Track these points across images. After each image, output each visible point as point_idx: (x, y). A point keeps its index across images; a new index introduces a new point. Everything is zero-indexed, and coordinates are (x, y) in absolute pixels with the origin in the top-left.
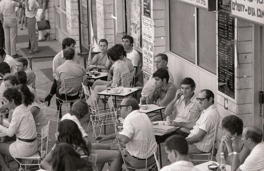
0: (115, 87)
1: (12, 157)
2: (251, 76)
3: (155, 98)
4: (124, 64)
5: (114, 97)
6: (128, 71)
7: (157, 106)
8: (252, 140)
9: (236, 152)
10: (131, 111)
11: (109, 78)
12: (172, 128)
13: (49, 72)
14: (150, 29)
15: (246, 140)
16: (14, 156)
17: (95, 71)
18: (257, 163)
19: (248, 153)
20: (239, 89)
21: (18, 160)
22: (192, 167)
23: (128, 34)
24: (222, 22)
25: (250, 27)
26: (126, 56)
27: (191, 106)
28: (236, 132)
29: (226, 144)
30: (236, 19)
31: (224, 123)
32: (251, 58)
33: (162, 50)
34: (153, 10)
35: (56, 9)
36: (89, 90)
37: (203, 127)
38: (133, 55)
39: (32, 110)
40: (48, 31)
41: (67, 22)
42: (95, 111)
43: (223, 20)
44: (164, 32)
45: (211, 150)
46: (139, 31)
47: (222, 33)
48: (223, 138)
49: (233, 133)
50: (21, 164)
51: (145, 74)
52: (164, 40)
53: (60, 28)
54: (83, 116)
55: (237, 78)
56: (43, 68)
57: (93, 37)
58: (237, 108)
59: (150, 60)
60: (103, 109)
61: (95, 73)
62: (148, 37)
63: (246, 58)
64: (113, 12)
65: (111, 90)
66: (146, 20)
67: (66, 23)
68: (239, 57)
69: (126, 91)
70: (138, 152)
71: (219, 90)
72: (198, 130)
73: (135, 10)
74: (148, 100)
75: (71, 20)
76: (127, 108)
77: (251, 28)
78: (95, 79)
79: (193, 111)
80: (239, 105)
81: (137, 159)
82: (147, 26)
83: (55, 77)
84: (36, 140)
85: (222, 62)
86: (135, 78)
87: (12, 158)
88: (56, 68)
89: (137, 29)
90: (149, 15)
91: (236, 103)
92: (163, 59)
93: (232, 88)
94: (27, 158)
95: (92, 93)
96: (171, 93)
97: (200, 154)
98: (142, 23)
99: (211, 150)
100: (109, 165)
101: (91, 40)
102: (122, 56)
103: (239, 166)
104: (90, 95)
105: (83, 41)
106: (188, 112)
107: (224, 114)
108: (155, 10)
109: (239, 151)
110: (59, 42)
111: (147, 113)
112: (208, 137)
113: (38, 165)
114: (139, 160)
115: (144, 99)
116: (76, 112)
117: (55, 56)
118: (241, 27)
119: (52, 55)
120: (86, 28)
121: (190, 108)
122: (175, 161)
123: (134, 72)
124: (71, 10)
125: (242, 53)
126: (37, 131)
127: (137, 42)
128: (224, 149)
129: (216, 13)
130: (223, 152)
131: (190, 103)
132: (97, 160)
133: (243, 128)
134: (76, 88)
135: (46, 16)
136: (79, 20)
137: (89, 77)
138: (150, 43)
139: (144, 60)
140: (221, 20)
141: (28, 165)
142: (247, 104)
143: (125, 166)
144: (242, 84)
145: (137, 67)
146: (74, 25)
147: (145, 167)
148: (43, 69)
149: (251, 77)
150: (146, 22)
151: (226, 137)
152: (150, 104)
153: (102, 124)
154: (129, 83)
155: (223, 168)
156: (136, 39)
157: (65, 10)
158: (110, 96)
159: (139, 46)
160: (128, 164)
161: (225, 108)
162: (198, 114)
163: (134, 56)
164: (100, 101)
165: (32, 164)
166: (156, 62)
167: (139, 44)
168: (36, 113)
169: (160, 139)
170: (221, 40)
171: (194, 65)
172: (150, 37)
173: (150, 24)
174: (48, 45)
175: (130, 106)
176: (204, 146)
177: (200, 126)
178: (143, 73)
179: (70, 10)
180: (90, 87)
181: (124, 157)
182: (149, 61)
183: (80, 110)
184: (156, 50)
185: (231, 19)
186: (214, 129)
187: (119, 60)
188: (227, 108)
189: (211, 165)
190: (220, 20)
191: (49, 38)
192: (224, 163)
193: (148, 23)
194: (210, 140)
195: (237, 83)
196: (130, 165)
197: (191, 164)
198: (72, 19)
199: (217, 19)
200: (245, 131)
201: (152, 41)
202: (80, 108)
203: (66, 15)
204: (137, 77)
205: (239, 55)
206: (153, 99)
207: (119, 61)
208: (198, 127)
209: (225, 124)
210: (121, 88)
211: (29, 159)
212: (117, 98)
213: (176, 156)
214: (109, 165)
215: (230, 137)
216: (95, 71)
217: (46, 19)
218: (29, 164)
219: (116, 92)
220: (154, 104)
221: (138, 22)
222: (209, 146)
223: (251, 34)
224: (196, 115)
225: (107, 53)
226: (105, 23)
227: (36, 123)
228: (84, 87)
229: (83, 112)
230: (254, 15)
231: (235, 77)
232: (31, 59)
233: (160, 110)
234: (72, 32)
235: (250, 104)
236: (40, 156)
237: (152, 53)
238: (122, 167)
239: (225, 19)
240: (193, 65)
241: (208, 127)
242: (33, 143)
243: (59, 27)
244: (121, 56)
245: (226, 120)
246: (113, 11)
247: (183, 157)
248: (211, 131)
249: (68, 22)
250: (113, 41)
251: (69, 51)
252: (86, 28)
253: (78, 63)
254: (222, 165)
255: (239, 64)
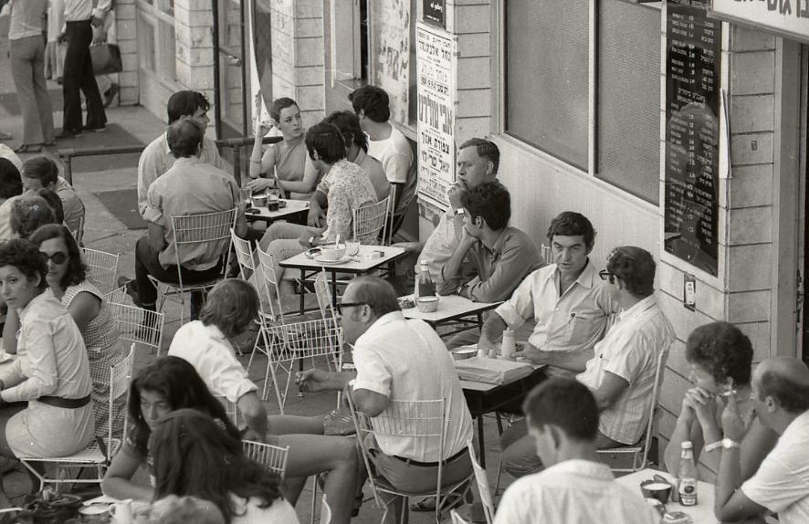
0: (335, 244)
1: (14, 458)
2: (768, 203)
3: (465, 272)
4: (360, 171)
5: (330, 273)
6: (371, 194)
7: (470, 301)
8: (780, 403)
9: (732, 439)
10: (371, 322)
11: (312, 217)
12: (520, 366)
13: (123, 204)
14: (444, 62)
15: (762, 402)
16: (23, 455)
17: (268, 194)
18: (798, 473)
19: (769, 442)
20: (731, 246)
21: (32, 466)
22: (608, 480)
23: (371, 82)
24: (680, 38)
25: (770, 50)
26: (366, 150)
27: (578, 298)
28: (729, 374)
29: (698, 413)
30: (726, 26)
31: (695, 344)
32: (770, 148)
33: (482, 130)
34: (455, 5)
35: (141, 9)
36: (253, 250)
37: (617, 366)
38: (394, 148)
39: (74, 309)
40: (114, 77)
41: (177, 49)
42: (272, 317)
43: (685, 29)
44: (487, 74)
45: (643, 437)
46: (406, 71)
47: (681, 71)
48: (687, 395)
49: (719, 379)
50: (43, 481)
51: (424, 205)
52: (487, 103)
53: (153, 68)
54: (242, 327)
55: (727, 211)
56: (101, 191)
57: (257, 93)
58: (725, 306)
59: (440, 161)
60: (296, 312)
61: (269, 202)
62: (437, 88)
63: (754, 146)
64: (322, 15)
65: (322, 251)
66: (431, 36)
67: (174, 49)
68: (733, 145)
69: (369, 255)
70: (406, 442)
71: (666, 249)
72: (603, 374)
73: (394, 7)
74: (442, 282)
75: (189, 43)
76: (357, 312)
77: (773, 53)
78: (270, 221)
79: (583, 313)
80: (731, 295)
81: (408, 461)
82: (433, 57)
83: (143, 213)
84: (91, 404)
85: (677, 163)
86: (394, 217)
87: (13, 461)
88: (147, 185)
89: (400, 65)
90: (441, 21)
91: (722, 288)
92: (481, 154)
93: (709, 241)
94: (63, 460)
95: (261, 260)
96: (515, 260)
97: (608, 449)
98: (418, 45)
99: (643, 437)
100: (322, 484)
101: (251, 105)
102: (354, 148)
103: (741, 484)
104: (257, 265)
105: (226, 110)
106: (569, 318)
107: (684, 326)
108: (459, 6)
109: (738, 438)
110: (148, 111)
111: (434, 325)
112: (632, 397)
113: (98, 484)
114: (412, 466)
115: (426, 280)
116: (220, 316)
117: (144, 148)
118: (741, 52)
119: (136, 146)
120: (237, 65)
121: (574, 306)
122: (555, 462)
123: (391, 199)
124: (191, 11)
125: (744, 133)
126: (93, 375)
127: (399, 108)
128: (692, 430)
129: (660, 10)
130: (690, 440)
131: (577, 289)
132: (288, 461)
133: (752, 366)
134: (212, 246)
135: (109, 32)
136: (214, 43)
137: (251, 214)
138: (444, 109)
139: (422, 162)
140: (678, 32)
141: (65, 481)
142: (757, 293)
143: (372, 485)
144: (742, 229)
145: (400, 187)
146: (198, 58)
147: (436, 489)
148: (101, 193)
149: (769, 209)
150: (430, 42)
151: (699, 392)
152: (449, 295)
153: (294, 357)
154: (376, 231)
155: (690, 490)
156: (396, 97)
157: (171, 13)
158: (318, 269)
159: (407, 119)
160: (382, 480)
161: (686, 306)
162: (602, 319)
163: (396, 152)
164: (287, 288)
165: (77, 478)
166: (460, 165)
167: (407, 113)
168: (85, 319)
169: (478, 402)
170: (675, 94)
171: (584, 174)
172: (443, 89)
173: (445, 49)
174: (116, 122)
175: (364, 304)
176: (620, 425)
177: (608, 361)
178: (418, 201)
179: (188, 13)
180: (256, 241)
181: (371, 455)
182: (439, 165)
183: (234, 309)
184: (461, 128)
185: (711, 25)
186: (652, 372)
187: (342, 158)
188: (694, 306)
189: (650, 482)
190: (674, 30)
191: (120, 101)
192: (691, 477)
193: (436, 45)
194: (641, 404)
195: (727, 225)
196: (389, 484)
197: (605, 470)
198: (192, 38)
199: (664, 28)
200: (757, 372)
201: (448, 101)
202: (232, 306)
203: (173, 28)
204: (399, 216)
205: (733, 138)
206: (458, 279)
207: (344, 162)
208: (601, 365)
209: (695, 349)
210: (352, 246)
211: (68, 463)
212: (339, 275)
213: (557, 445)
214: (322, 484)
215: (708, 392)
216: (268, 194)
217: (111, 40)
218: (67, 479)
219: (338, 258)
220: (459, 295)
221: (402, 43)
222: (636, 425)
223: (773, 72)
224: (591, 329)
225: (306, 142)
226: (298, 48)
227: (87, 347)
228: (236, 241)
229: (240, 317)
230: (787, 12)
231: (720, 209)
232: (71, 156)
233: (478, 312)
234: (194, 74)
235: (766, 292)
236: (105, 454)
237: (449, 140)
238: (363, 491)
239: (692, 26)
240: (581, 176)
241: (632, 369)
242: (82, 410)
243: (149, 65)
244: (349, 146)
245: (701, 336)
246: (324, 13)
247: (580, 447)
248: (643, 379)
249: (181, 49)
250: (321, 105)
251: (184, 129)
252: (237, 65)
253: (216, 166)
254: (684, 480)
255: (732, 166)
